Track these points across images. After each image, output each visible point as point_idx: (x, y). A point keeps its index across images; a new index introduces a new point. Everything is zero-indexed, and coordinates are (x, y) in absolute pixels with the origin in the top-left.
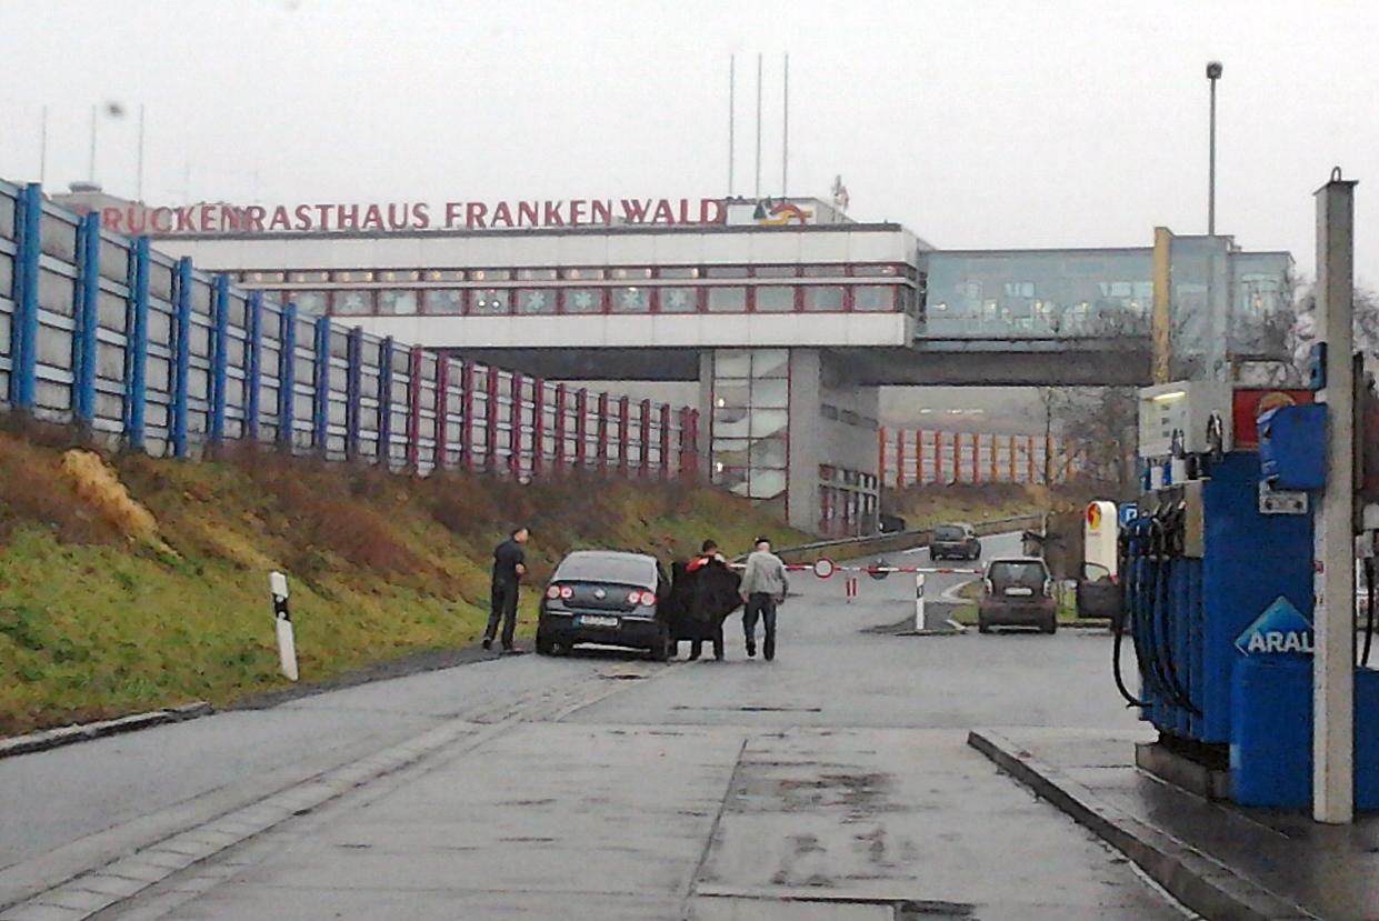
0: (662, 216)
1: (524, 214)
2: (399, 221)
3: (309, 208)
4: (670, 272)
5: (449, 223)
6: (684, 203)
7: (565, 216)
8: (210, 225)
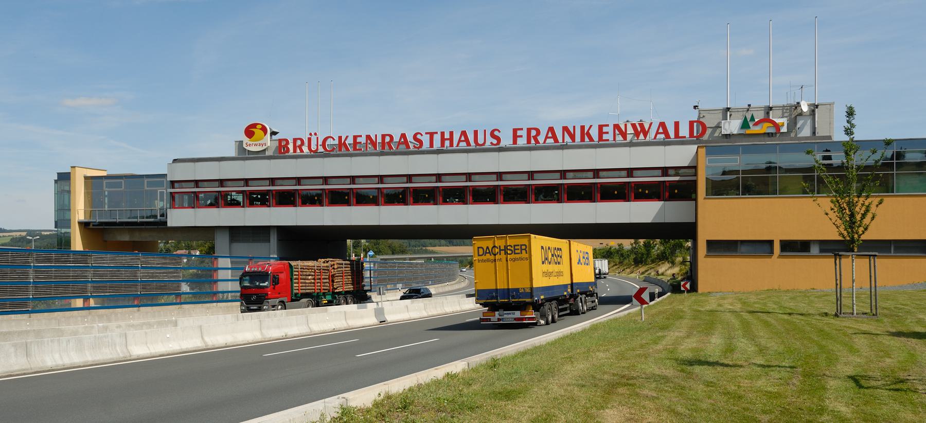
0: (550, 138)
1: (566, 135)
2: (481, 141)
3: (422, 135)
4: (509, 176)
5: (515, 142)
6: (677, 124)
7: (594, 133)
8: (605, 137)
